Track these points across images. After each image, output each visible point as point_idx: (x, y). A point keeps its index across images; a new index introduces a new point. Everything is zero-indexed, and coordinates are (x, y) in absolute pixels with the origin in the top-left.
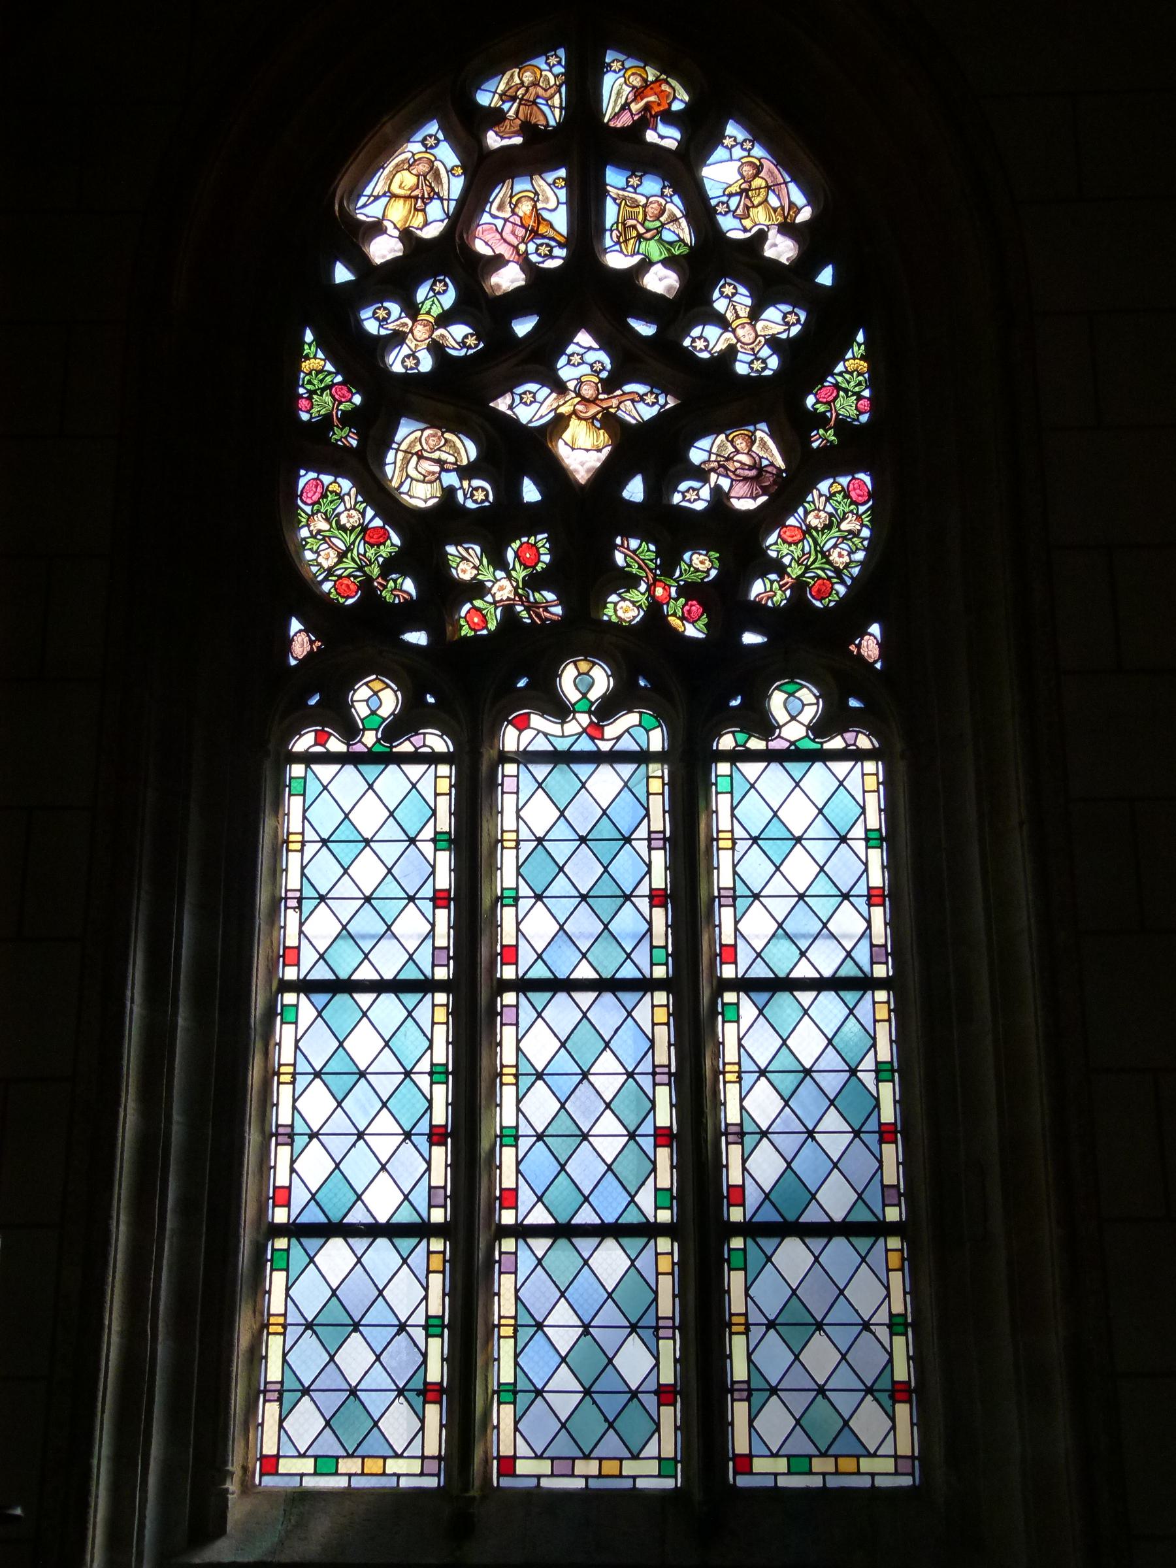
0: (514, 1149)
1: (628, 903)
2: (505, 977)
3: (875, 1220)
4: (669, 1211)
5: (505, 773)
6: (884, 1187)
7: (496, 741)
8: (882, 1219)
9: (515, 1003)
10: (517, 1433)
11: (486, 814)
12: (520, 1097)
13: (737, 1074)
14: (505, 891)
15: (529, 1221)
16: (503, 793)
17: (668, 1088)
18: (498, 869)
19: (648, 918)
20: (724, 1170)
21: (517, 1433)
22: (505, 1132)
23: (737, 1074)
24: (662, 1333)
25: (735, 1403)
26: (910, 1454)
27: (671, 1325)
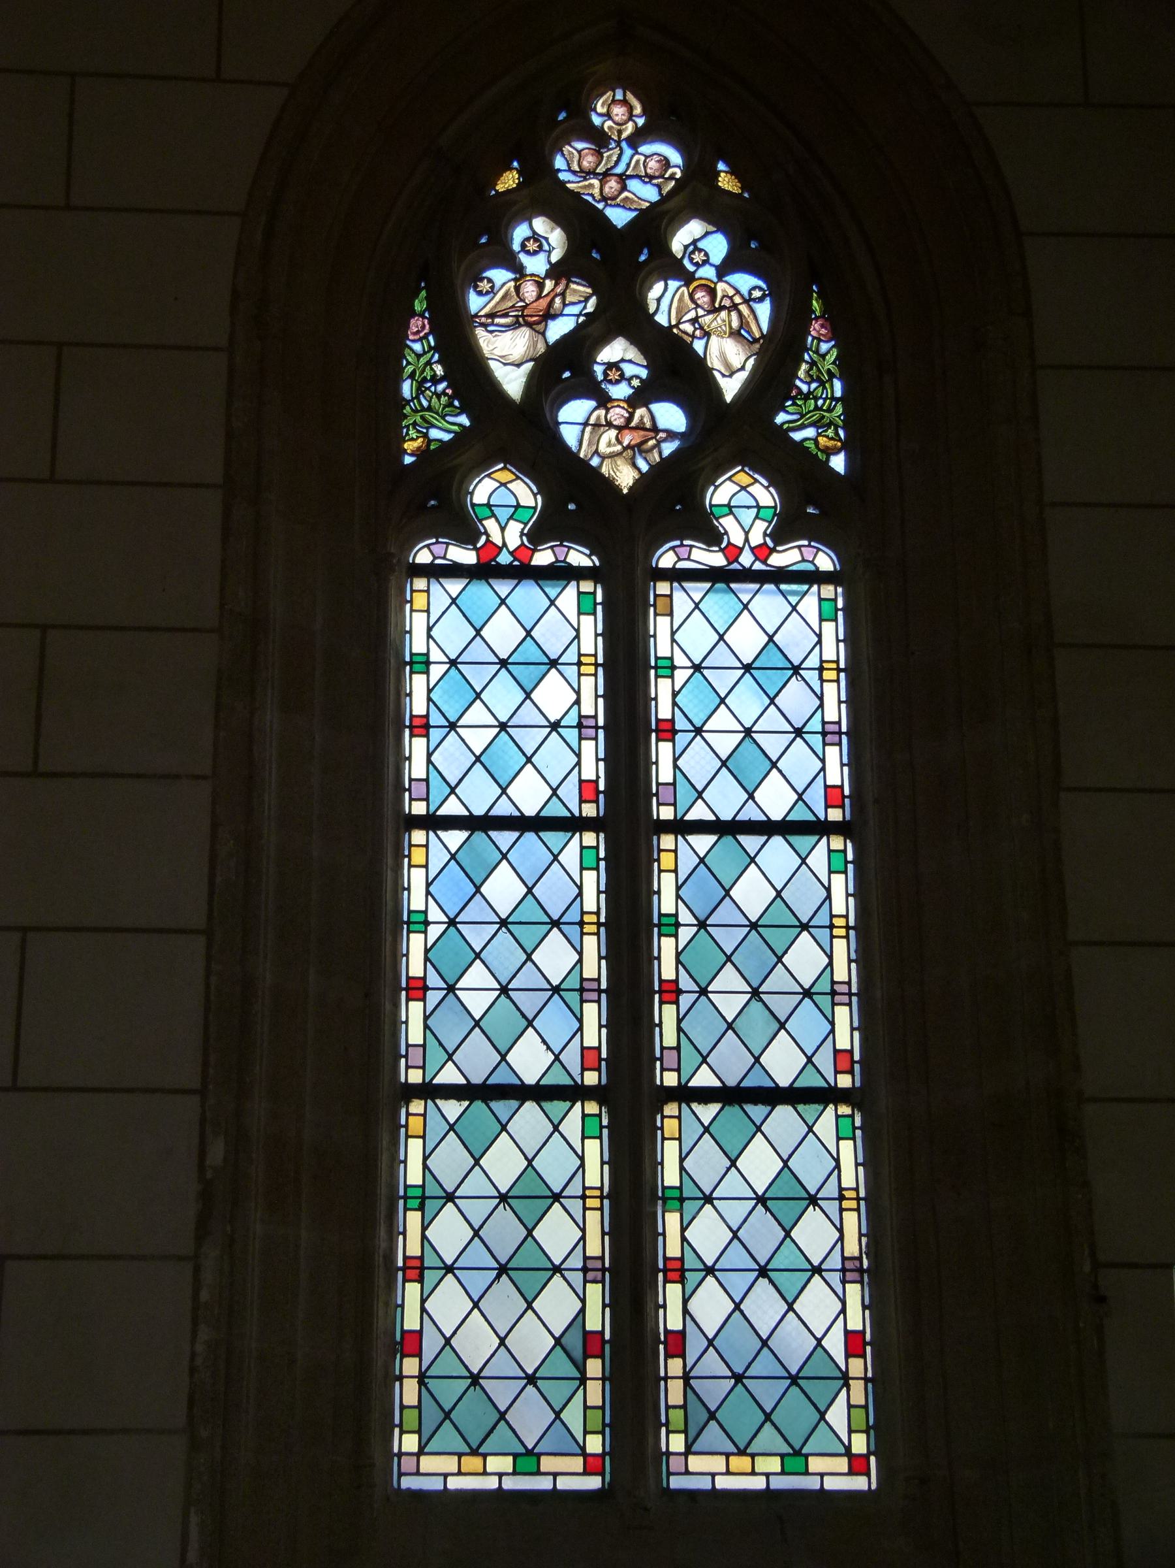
0: (423, 936)
1: (557, 1204)
2: (410, 1081)
3: (826, 1086)
4: (596, 1073)
5: (403, 1470)
6: (836, 1052)
7: (394, 1296)
8: (833, 1085)
9: (425, 777)
10: (429, 897)
11: (393, 602)
12: (425, 1315)
13: (679, 1273)
14: (409, 1189)
15: (442, 812)
16: (410, 866)
17: (600, 1436)
18: (405, 889)
19: (580, 1153)
20: (656, 962)
21: (429, 897)
22: (416, 659)
23: (679, 1273)
24: (587, 929)
25: (663, 939)
26: (847, 996)
27: (593, 662)
